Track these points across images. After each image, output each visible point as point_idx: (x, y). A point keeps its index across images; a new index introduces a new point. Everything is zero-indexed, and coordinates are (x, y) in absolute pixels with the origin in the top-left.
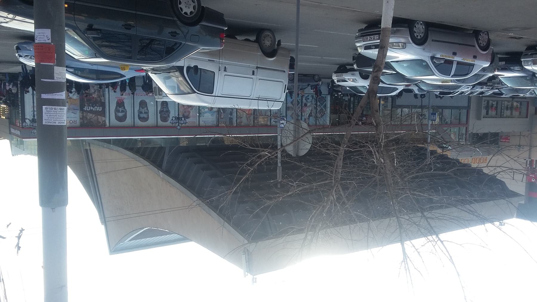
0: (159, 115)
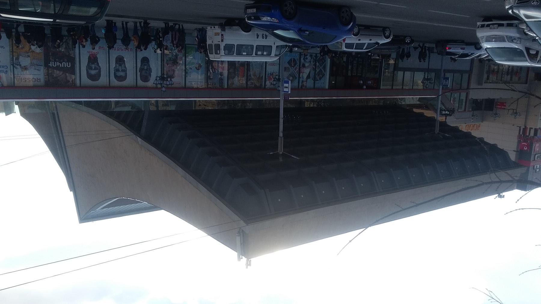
0: (139, 74)
